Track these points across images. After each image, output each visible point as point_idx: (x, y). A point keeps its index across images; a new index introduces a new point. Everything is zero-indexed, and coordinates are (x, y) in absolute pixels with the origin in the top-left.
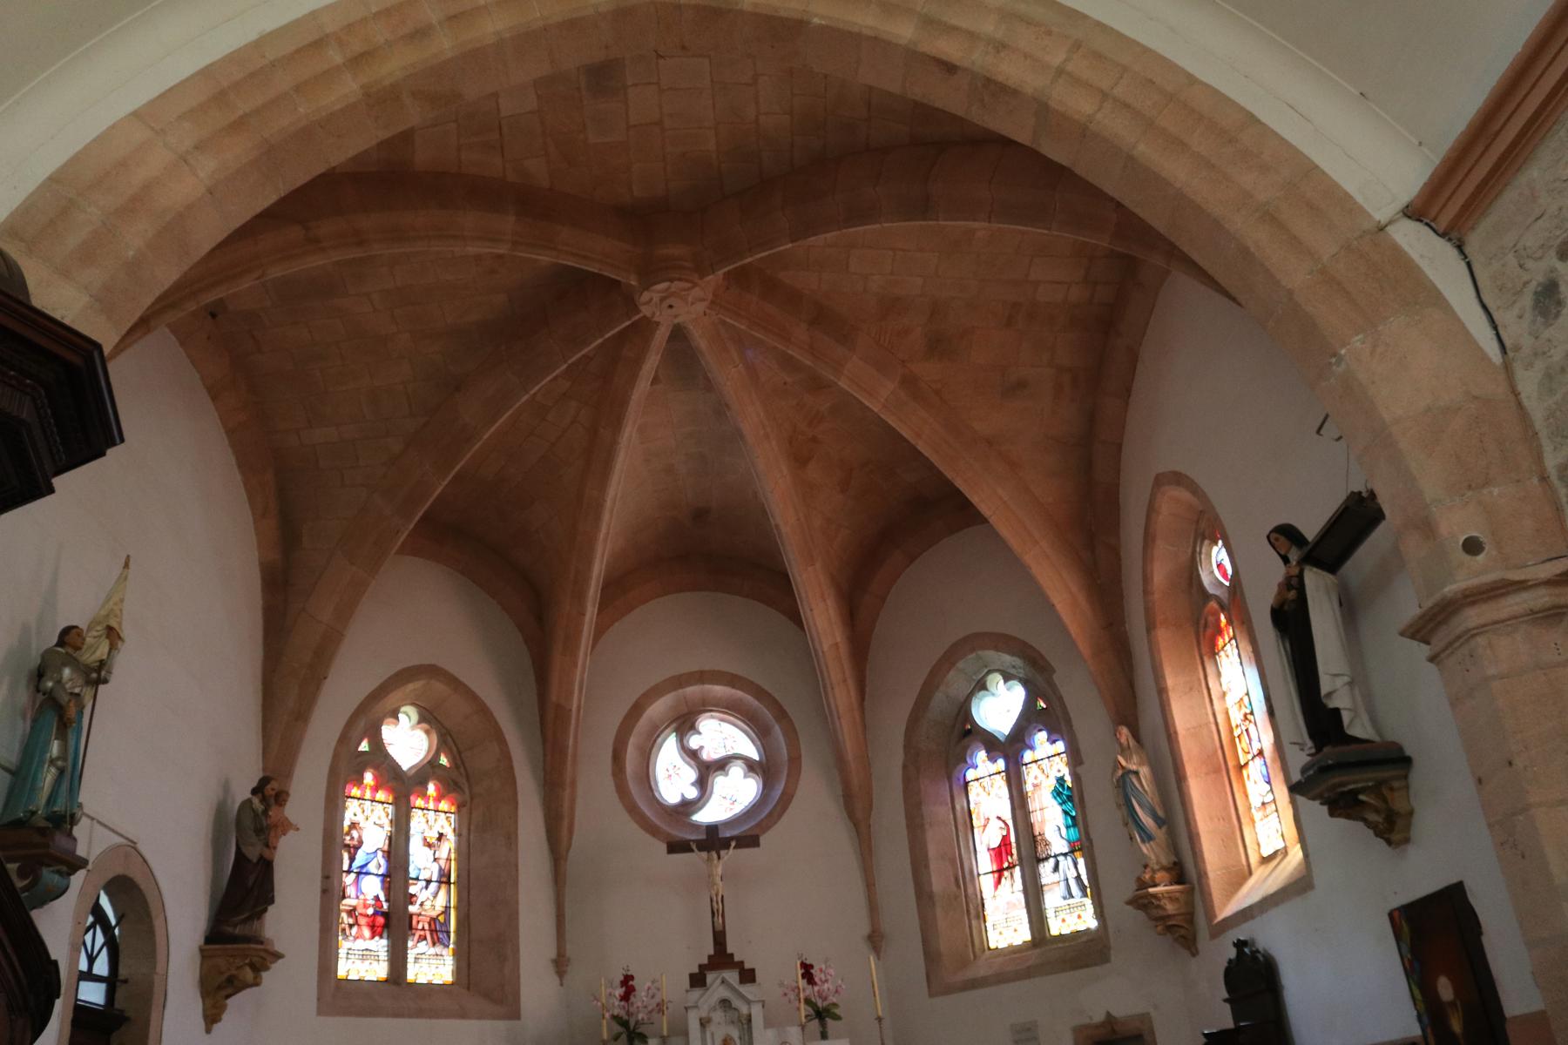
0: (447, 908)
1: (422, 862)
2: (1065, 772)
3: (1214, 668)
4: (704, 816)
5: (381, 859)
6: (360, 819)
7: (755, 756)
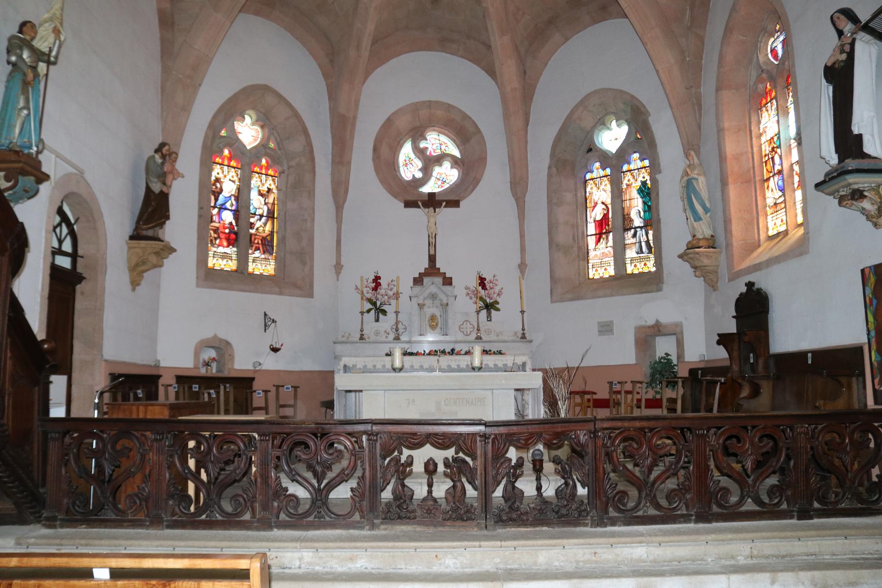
0: (272, 233)
1: (256, 202)
3: (756, 118)
4: (426, 189)
6: (221, 176)
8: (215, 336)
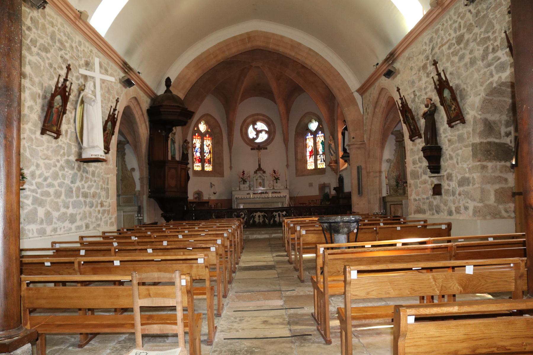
0: (211, 158)
1: (206, 149)
2: (323, 139)
5: (199, 149)
7: (267, 130)
8: (198, 190)
